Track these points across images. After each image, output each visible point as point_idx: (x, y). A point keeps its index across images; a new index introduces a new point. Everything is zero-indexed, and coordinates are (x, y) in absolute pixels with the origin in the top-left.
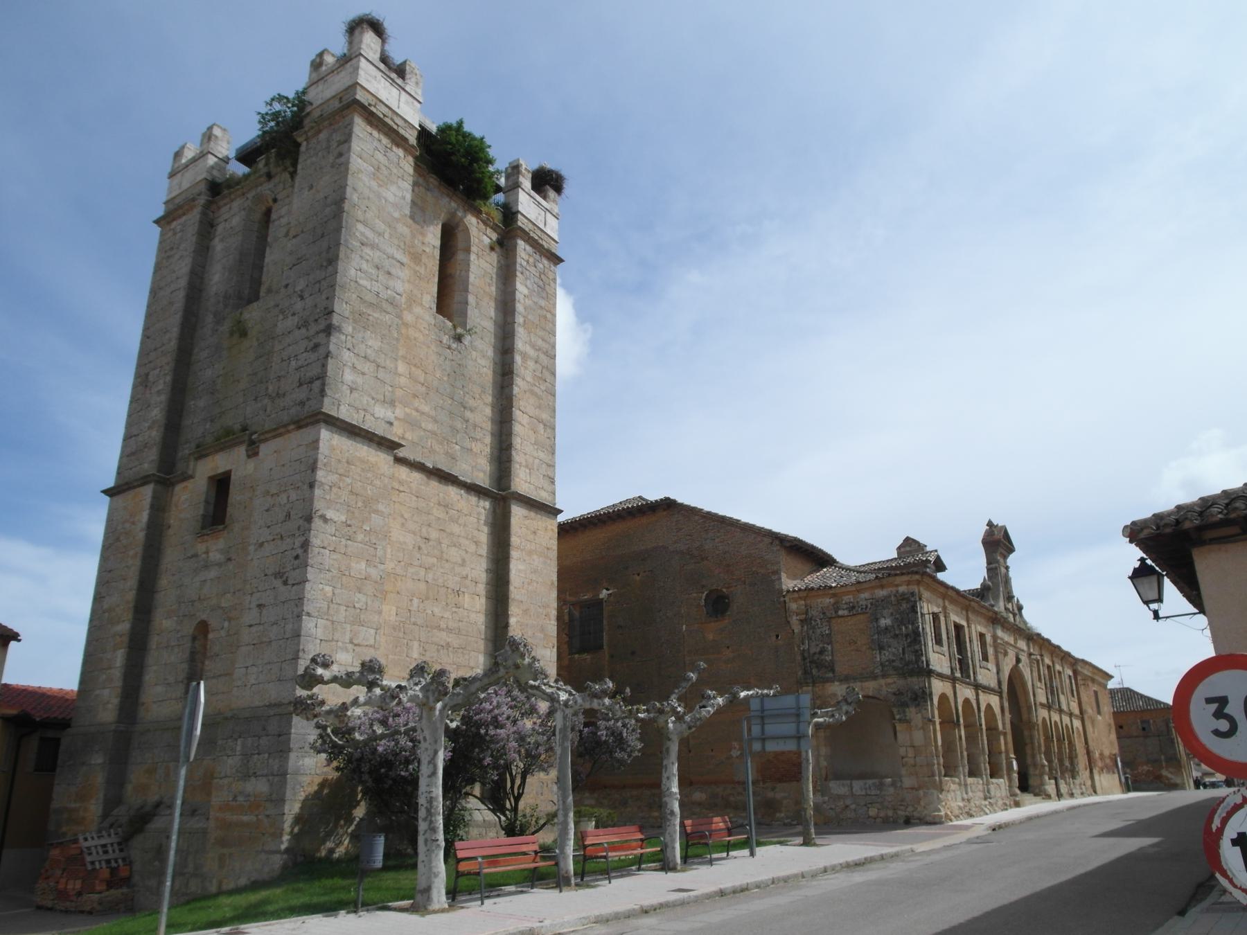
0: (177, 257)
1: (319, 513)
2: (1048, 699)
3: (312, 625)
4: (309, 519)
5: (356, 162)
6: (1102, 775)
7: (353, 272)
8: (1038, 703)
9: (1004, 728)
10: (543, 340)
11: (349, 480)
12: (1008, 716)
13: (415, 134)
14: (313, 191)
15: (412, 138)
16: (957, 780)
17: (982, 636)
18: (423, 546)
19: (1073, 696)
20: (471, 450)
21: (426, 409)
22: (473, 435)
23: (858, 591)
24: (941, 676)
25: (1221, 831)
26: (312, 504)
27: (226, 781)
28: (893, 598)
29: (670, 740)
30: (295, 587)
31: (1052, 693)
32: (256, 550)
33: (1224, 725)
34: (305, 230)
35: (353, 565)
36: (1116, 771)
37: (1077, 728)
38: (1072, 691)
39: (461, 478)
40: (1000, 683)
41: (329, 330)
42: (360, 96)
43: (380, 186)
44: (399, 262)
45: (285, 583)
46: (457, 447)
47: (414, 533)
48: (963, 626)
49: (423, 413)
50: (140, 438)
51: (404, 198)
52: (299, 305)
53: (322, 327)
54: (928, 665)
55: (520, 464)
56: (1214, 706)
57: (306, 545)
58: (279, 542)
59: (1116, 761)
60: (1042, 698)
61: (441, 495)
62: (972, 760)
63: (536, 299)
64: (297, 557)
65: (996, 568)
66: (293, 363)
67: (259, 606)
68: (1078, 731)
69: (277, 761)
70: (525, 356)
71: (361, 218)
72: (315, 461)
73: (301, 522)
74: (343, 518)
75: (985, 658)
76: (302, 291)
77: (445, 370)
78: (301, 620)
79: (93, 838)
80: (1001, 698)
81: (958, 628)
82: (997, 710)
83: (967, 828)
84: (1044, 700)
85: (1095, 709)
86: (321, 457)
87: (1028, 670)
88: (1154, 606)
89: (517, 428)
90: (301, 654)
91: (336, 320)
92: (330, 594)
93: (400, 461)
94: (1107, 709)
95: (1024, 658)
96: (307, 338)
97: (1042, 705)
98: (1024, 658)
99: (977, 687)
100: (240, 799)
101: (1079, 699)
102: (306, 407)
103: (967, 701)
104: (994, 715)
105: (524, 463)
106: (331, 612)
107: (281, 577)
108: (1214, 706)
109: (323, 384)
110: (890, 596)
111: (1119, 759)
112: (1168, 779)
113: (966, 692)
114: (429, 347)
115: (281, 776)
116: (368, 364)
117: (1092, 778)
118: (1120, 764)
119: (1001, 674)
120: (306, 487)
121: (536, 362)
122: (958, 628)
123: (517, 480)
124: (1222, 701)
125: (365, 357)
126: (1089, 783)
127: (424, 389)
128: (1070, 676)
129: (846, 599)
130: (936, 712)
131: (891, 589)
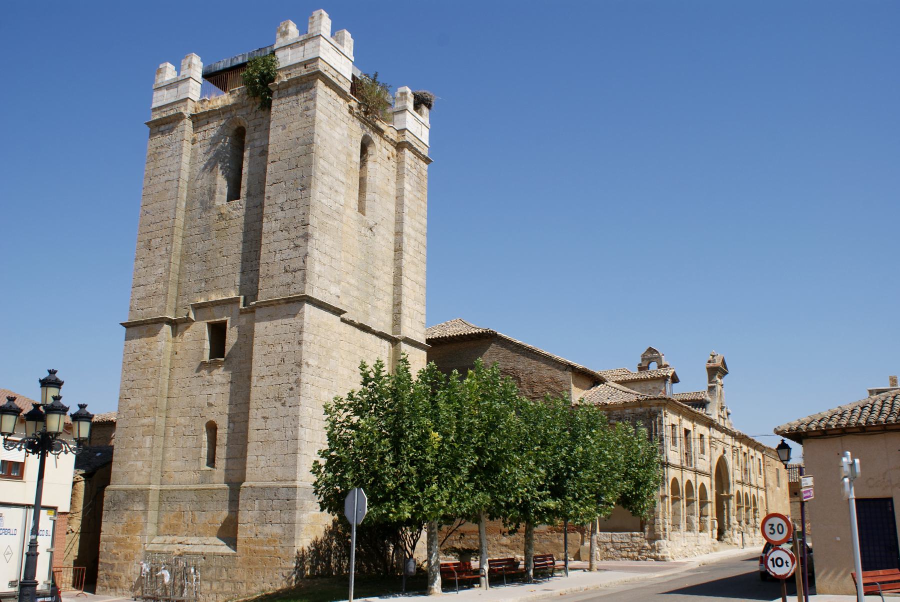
0: (167, 155)
1: (305, 361)
2: (742, 477)
3: (303, 433)
4: (299, 365)
5: (320, 115)
7: (318, 194)
8: (735, 481)
9: (711, 499)
10: (419, 223)
11: (318, 338)
12: (714, 490)
13: (349, 85)
14: (287, 130)
15: (347, 88)
16: (679, 534)
18: (352, 376)
19: (761, 474)
20: (377, 307)
21: (353, 281)
22: (378, 296)
23: (624, 408)
24: (674, 466)
25: (768, 557)
26: (301, 355)
27: (248, 525)
28: (647, 414)
29: (11, 406)
30: (292, 408)
31: (746, 473)
32: (258, 380)
33: (772, 531)
34: (281, 159)
35: (322, 393)
37: (761, 497)
38: (760, 469)
39: (373, 328)
40: (711, 468)
41: (306, 237)
42: (321, 66)
43: (331, 129)
44: (341, 182)
45: (284, 405)
46: (370, 306)
47: (348, 368)
49: (351, 285)
50: (148, 288)
51: (343, 135)
52: (280, 214)
53: (301, 234)
54: (667, 460)
55: (406, 315)
56: (770, 526)
57: (298, 382)
58: (277, 378)
61: (361, 340)
62: (689, 521)
63: (415, 193)
64: (291, 389)
65: (714, 387)
66: (278, 255)
67: (264, 418)
69: (287, 515)
70: (409, 236)
71: (322, 155)
72: (302, 327)
73: (294, 366)
74: (316, 363)
75: (703, 452)
76: (282, 204)
77: (363, 252)
78: (297, 430)
80: (711, 478)
81: (687, 432)
82: (708, 487)
83: (684, 564)
84: (739, 479)
85: (776, 482)
86: (305, 324)
87: (731, 458)
88: (785, 462)
89: (405, 290)
90: (298, 451)
91: (310, 229)
92: (311, 413)
93: (343, 320)
95: (729, 450)
96: (289, 239)
97: (738, 482)
98: (729, 450)
99: (696, 472)
100: (260, 536)
101: (765, 476)
102: (292, 289)
103: (689, 482)
104: (705, 490)
105: (408, 315)
106: (312, 424)
107: (280, 400)
108: (770, 526)
109: (305, 275)
110: (645, 413)
113: (689, 476)
114: (354, 237)
115: (291, 526)
116: (327, 257)
119: (712, 461)
120: (295, 343)
121: (415, 240)
122: (687, 432)
123: (404, 326)
124: (772, 525)
125: (325, 253)
127: (352, 267)
128: (759, 459)
129: (616, 412)
130: (670, 490)
131: (646, 408)
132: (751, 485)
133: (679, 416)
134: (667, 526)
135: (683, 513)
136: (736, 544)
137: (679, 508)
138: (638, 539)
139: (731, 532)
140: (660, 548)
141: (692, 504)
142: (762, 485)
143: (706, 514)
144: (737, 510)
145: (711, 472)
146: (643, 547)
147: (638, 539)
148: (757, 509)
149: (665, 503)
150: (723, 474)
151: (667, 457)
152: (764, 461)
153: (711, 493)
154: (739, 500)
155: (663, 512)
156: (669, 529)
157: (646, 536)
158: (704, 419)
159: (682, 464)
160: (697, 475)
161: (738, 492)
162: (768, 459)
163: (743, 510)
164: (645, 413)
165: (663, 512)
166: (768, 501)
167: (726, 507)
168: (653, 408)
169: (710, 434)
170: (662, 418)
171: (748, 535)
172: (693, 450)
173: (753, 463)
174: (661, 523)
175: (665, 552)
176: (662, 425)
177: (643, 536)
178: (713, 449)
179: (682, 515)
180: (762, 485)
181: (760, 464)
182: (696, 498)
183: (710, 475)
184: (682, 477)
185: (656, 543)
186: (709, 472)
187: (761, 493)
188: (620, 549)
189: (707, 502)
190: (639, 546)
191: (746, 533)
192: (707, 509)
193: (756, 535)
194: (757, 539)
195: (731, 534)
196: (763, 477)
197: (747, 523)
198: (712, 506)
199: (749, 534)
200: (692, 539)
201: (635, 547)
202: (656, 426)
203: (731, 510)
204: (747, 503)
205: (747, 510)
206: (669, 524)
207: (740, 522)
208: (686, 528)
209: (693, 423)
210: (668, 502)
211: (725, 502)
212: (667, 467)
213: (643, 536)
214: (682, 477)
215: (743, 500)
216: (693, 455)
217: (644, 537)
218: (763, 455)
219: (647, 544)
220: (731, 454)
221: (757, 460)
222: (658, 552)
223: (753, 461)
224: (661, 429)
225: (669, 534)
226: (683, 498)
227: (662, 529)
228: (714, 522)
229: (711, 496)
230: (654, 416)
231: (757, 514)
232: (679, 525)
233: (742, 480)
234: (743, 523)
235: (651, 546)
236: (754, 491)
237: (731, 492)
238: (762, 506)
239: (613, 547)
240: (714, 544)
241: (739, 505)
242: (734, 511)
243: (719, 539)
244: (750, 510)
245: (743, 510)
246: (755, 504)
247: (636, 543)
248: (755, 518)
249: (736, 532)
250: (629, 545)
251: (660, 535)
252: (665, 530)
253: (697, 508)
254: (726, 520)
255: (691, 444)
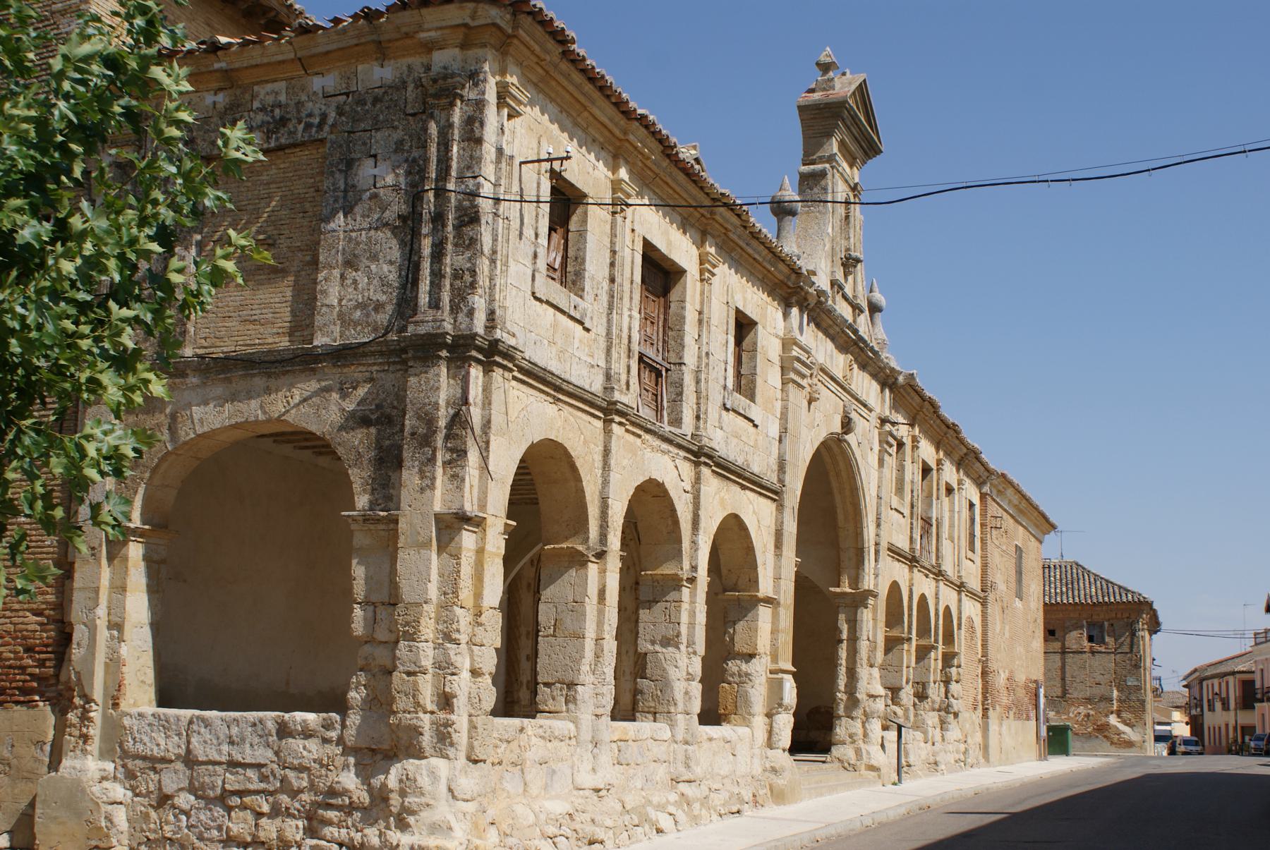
6: (1005, 723)
8: (884, 545)
9: (777, 591)
17: (744, 326)
19: (973, 551)
28: (411, 93)
36: (1033, 714)
37: (970, 619)
38: (972, 535)
48: (681, 272)
59: (1037, 696)
60: (898, 532)
65: (823, 174)
68: (972, 628)
79: (1226, 707)
80: (780, 507)
82: (762, 540)
84: (903, 543)
85: (1013, 585)
87: (873, 459)
94: (1034, 587)
97: (895, 552)
99: (700, 455)
101: (984, 558)
110: (404, 84)
111: (1042, 691)
112: (1119, 733)
117: (985, 729)
118: (1042, 700)
119: (787, 441)
126: (978, 737)
132: (939, 574)
133: (614, 169)
134: (462, 684)
135: (600, 624)
136: (872, 768)
137: (579, 602)
138: (310, 750)
139: (858, 724)
140: (411, 800)
141: (672, 596)
142: (974, 584)
143: (746, 650)
144: (888, 650)
145: (781, 481)
146: (332, 792)
147: (310, 750)
148: (954, 655)
149: (457, 557)
150: (840, 517)
151: (491, 314)
152: (984, 513)
153: (777, 567)
154: (894, 615)
155: (446, 606)
156: (471, 700)
157: (351, 733)
158: (761, 254)
159: (608, 389)
160: (705, 471)
161: (895, 587)
162: (993, 509)
163: (908, 653)
164: (404, 84)
165: (446, 606)
166: (990, 634)
167: (844, 636)
168: (441, 58)
169: (788, 330)
170: (480, 104)
171: (919, 735)
172: (690, 357)
173: (952, 511)
174: (427, 662)
175: (434, 828)
176: (479, 141)
177: (333, 735)
178: (798, 398)
179: (590, 633)
180: (974, 584)
181: (972, 520)
182: (694, 568)
183: (774, 493)
184: (607, 452)
185: (392, 779)
186: (771, 478)
187: (971, 609)
188: (222, 799)
189: (756, 601)
190: (312, 787)
191: (916, 727)
192: (754, 630)
193: (948, 735)
194: (950, 747)
195: (860, 731)
196: (978, 560)
197: (921, 696)
198: (775, 617)
199: (925, 733)
200: (659, 750)
201: (294, 794)
202: (445, 145)
203: (863, 646)
204: (924, 630)
205: (923, 653)
206: (475, 673)
207: (894, 691)
208: (608, 702)
209: (700, 244)
210: (480, 551)
211: (842, 617)
212: (488, 367)
213: (333, 735)
214: (607, 452)
215: (911, 619)
216: (688, 380)
217: (340, 741)
218: (983, 497)
219: (349, 780)
220: (876, 448)
221: (965, 505)
222: (403, 826)
223: (952, 503)
224: (472, 164)
225: (472, 727)
226: (601, 555)
227: (427, 697)
228: (781, 682)
229: (777, 578)
230: (437, 96)
231: (954, 670)
232: (571, 685)
233: (912, 550)
234: (907, 694)
235: (370, 790)
236: (949, 596)
237: (868, 583)
238: (971, 647)
239: (192, 790)
240: (774, 770)
241: (895, 633)
242: (873, 649)
243: (797, 747)
244: (933, 654)
245: (908, 653)
246: (949, 638)
247: (301, 769)
248: (947, 682)
249: (875, 726)
250: (263, 778)
251: (416, 731)
252: (446, 701)
253: (692, 614)
254: (842, 681)
255: (681, 331)
